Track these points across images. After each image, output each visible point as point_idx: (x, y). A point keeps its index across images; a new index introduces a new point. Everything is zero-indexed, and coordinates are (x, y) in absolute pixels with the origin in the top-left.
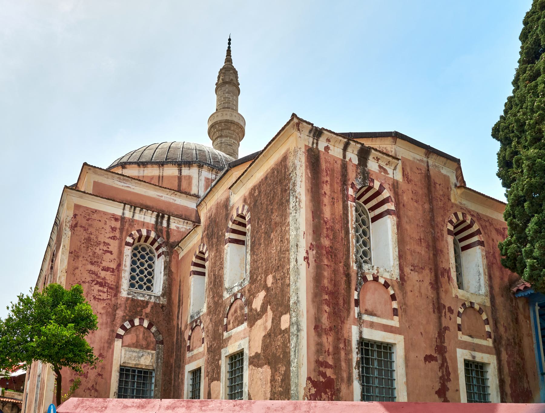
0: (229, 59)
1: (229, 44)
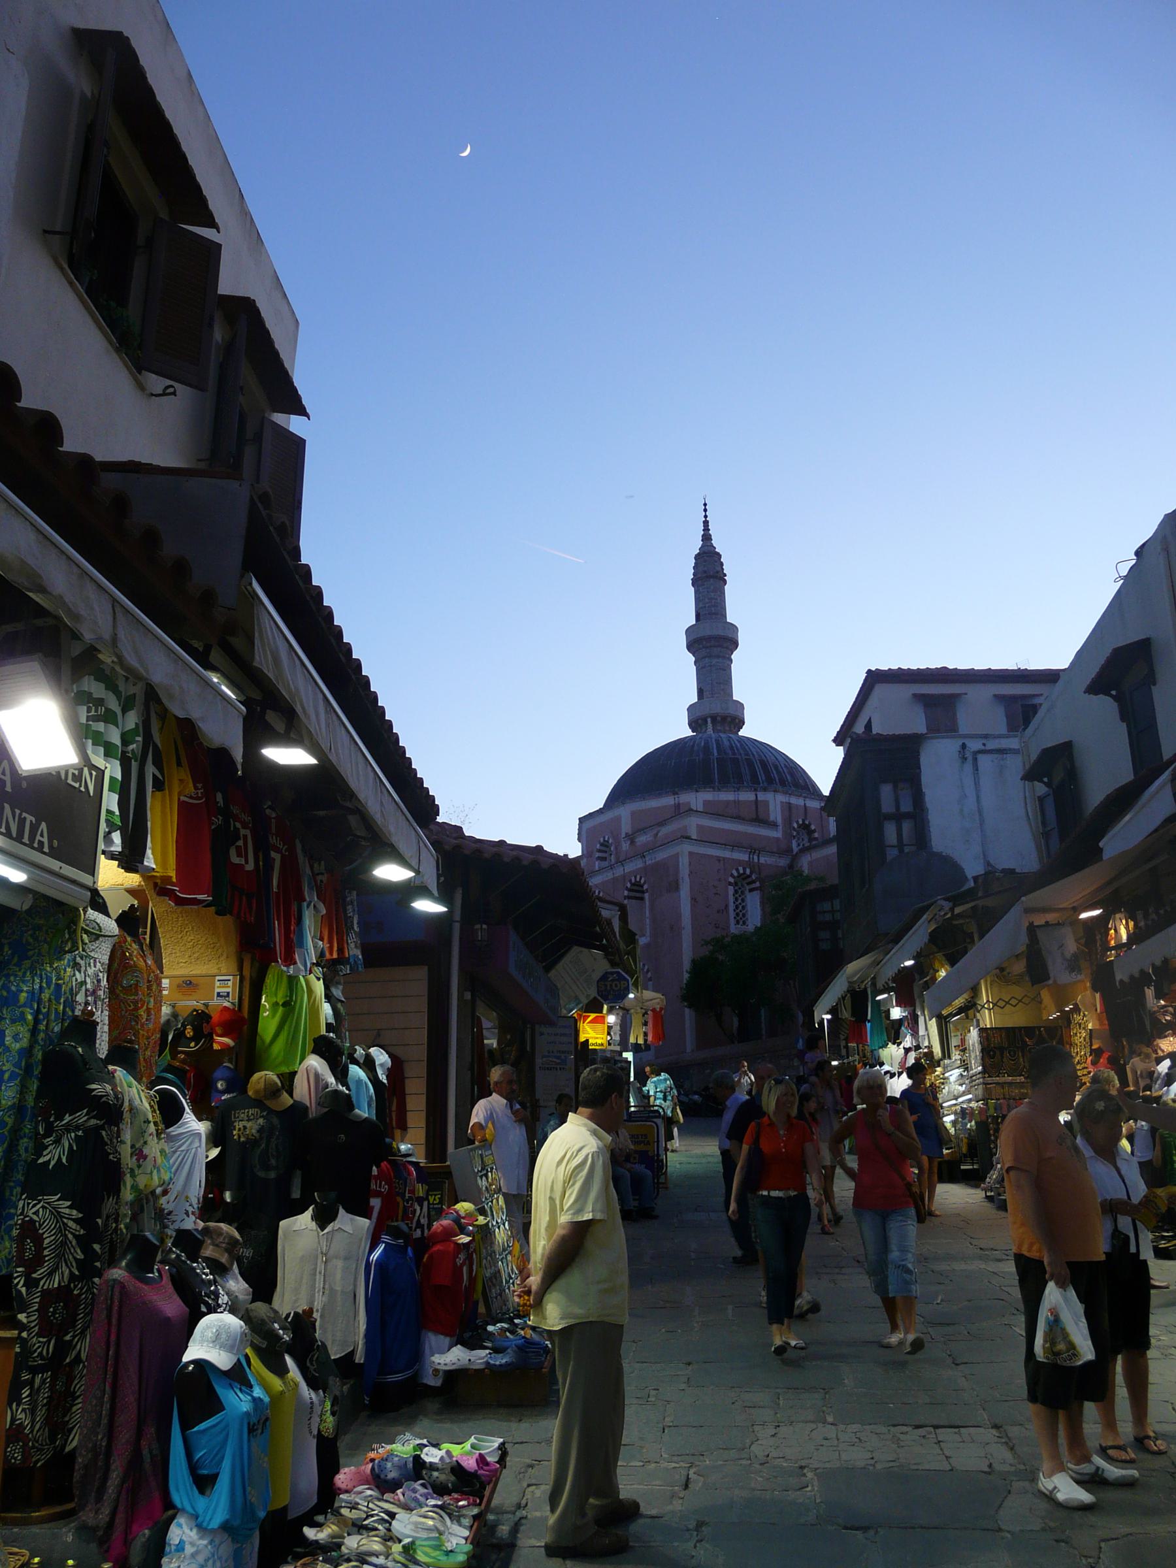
0: (707, 537)
1: (705, 510)
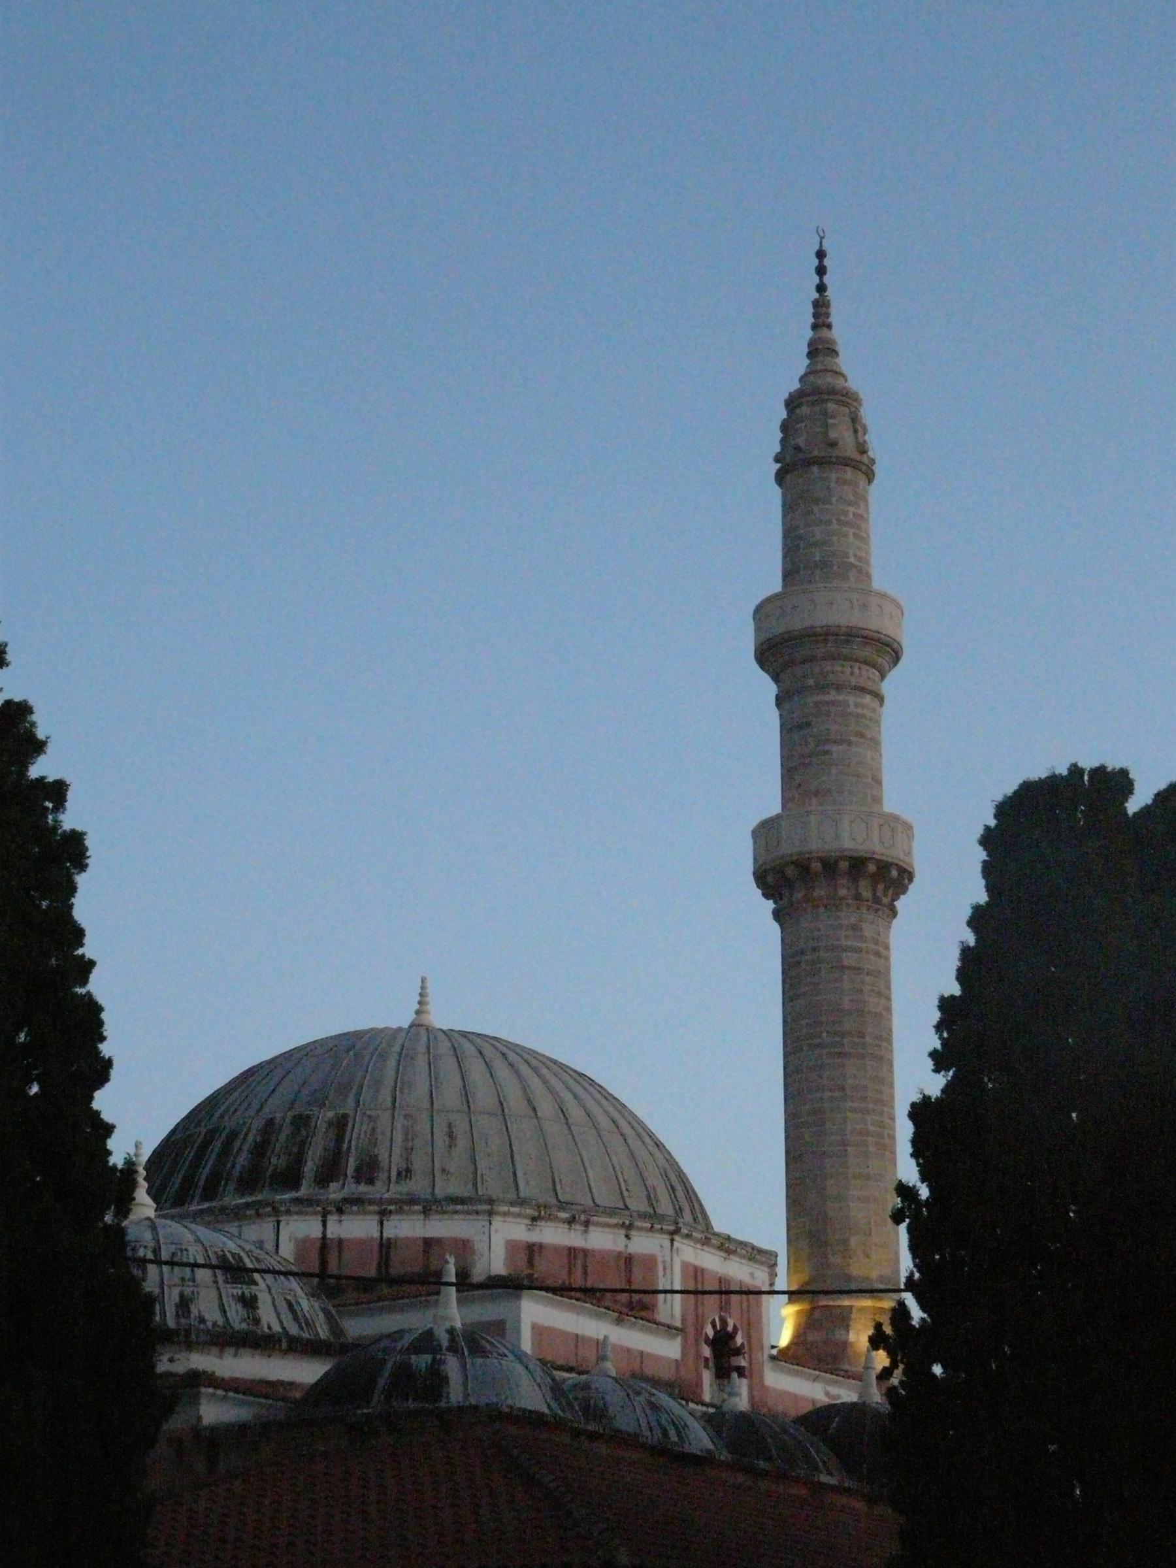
0: (821, 349)
1: (821, 271)
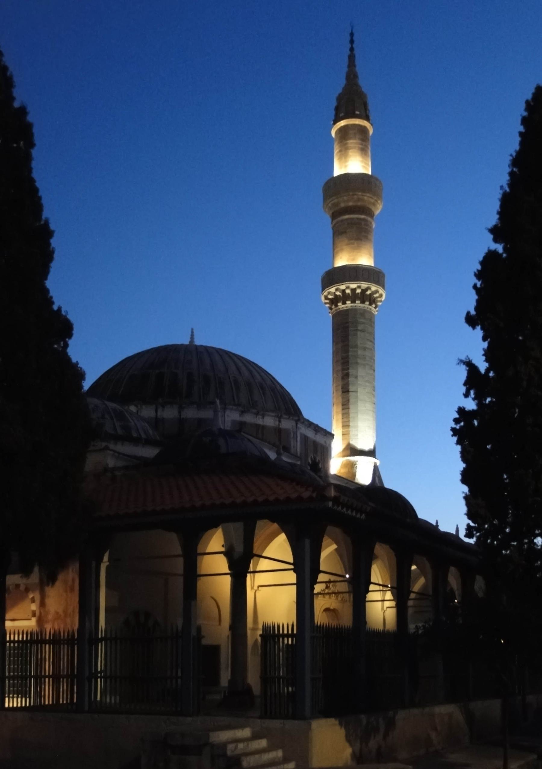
1: (352, 42)
